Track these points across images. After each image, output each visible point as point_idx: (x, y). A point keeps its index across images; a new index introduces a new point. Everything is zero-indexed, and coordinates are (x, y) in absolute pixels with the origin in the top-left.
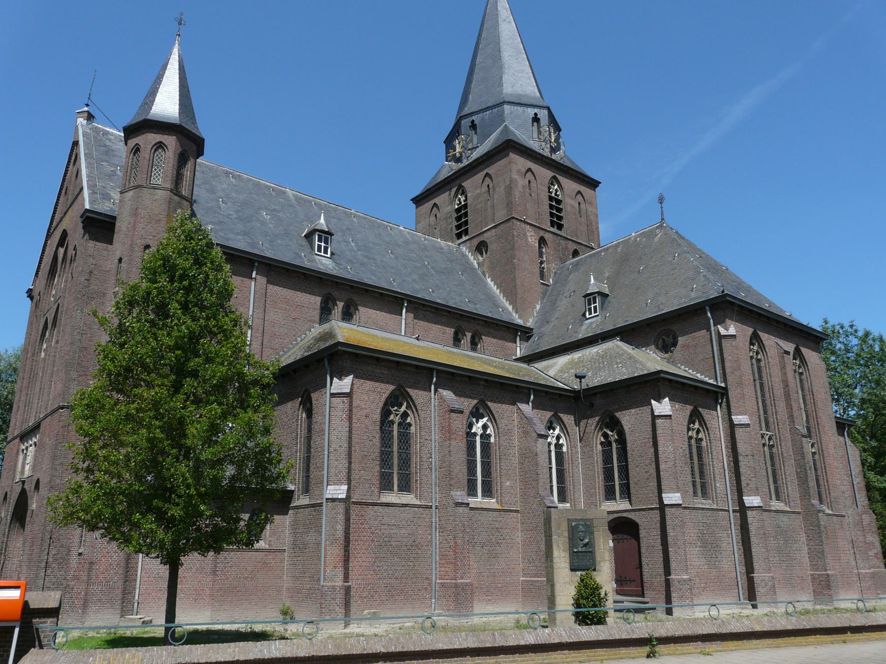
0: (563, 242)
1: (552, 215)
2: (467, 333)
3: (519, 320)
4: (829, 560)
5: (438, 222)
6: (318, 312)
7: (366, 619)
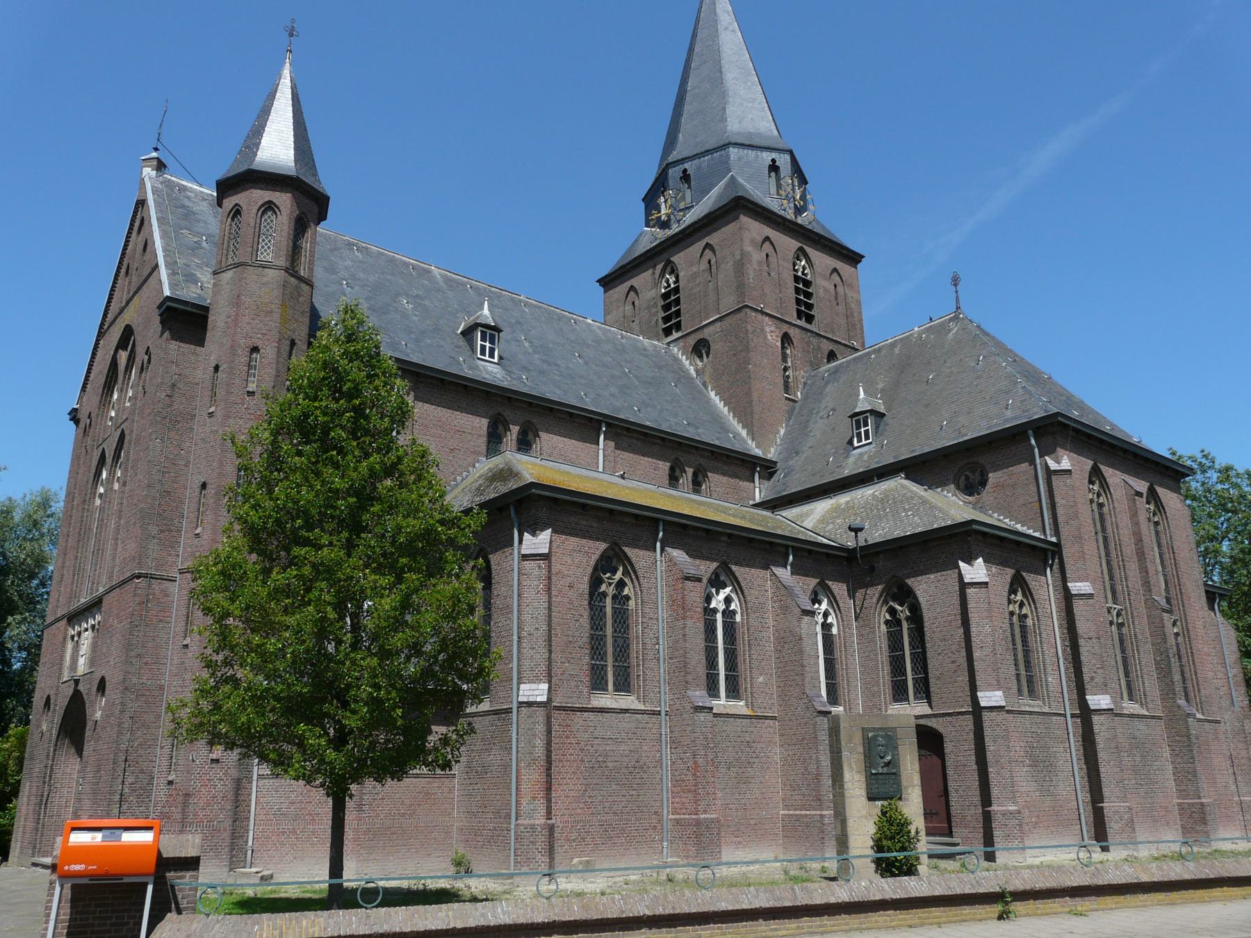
0: (814, 340)
1: (798, 302)
2: (687, 469)
3: (756, 450)
4: (1203, 784)
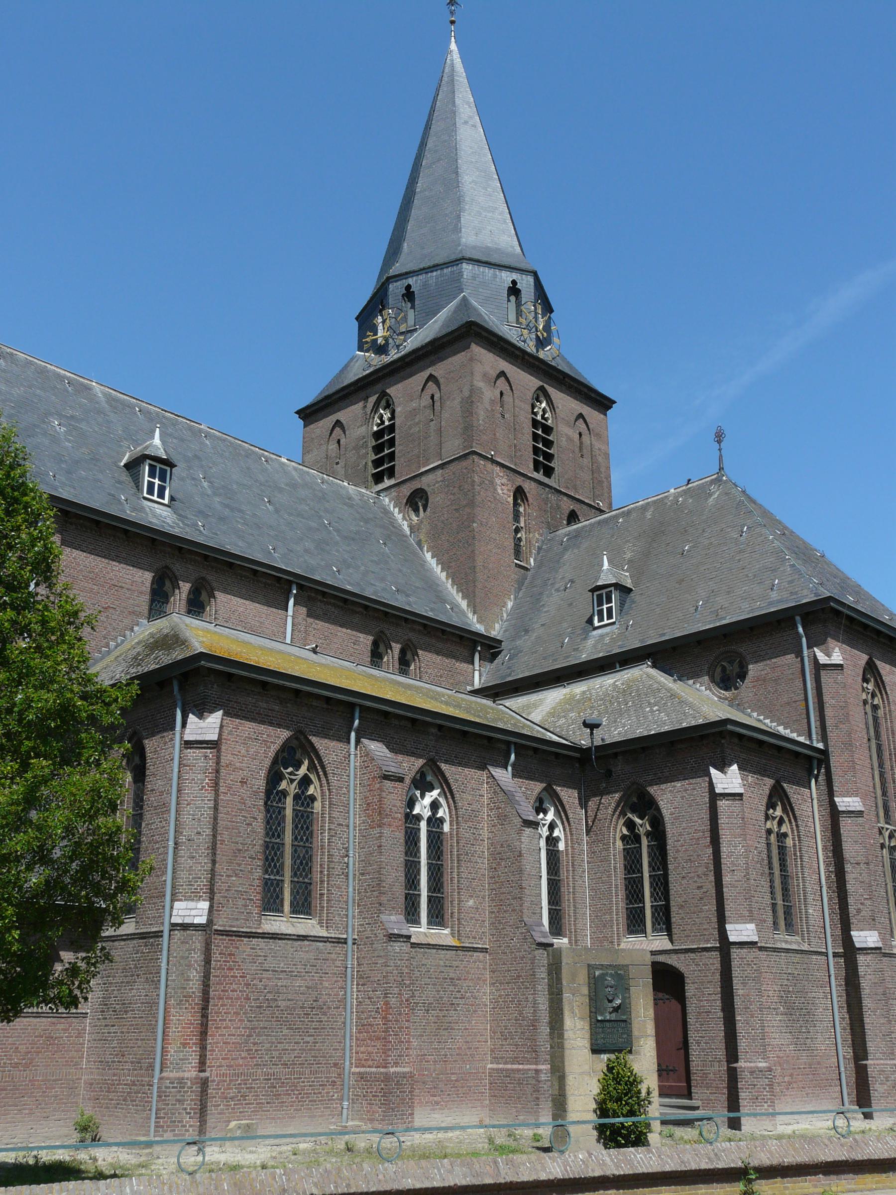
0: (553, 497)
1: (536, 450)
2: (393, 645)
5: (342, 453)
6: (147, 597)
7: (232, 1139)
